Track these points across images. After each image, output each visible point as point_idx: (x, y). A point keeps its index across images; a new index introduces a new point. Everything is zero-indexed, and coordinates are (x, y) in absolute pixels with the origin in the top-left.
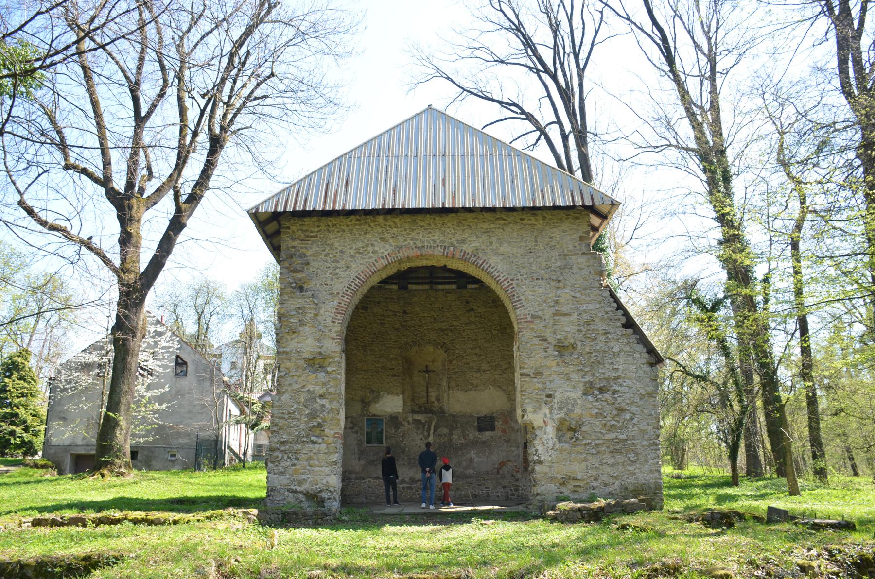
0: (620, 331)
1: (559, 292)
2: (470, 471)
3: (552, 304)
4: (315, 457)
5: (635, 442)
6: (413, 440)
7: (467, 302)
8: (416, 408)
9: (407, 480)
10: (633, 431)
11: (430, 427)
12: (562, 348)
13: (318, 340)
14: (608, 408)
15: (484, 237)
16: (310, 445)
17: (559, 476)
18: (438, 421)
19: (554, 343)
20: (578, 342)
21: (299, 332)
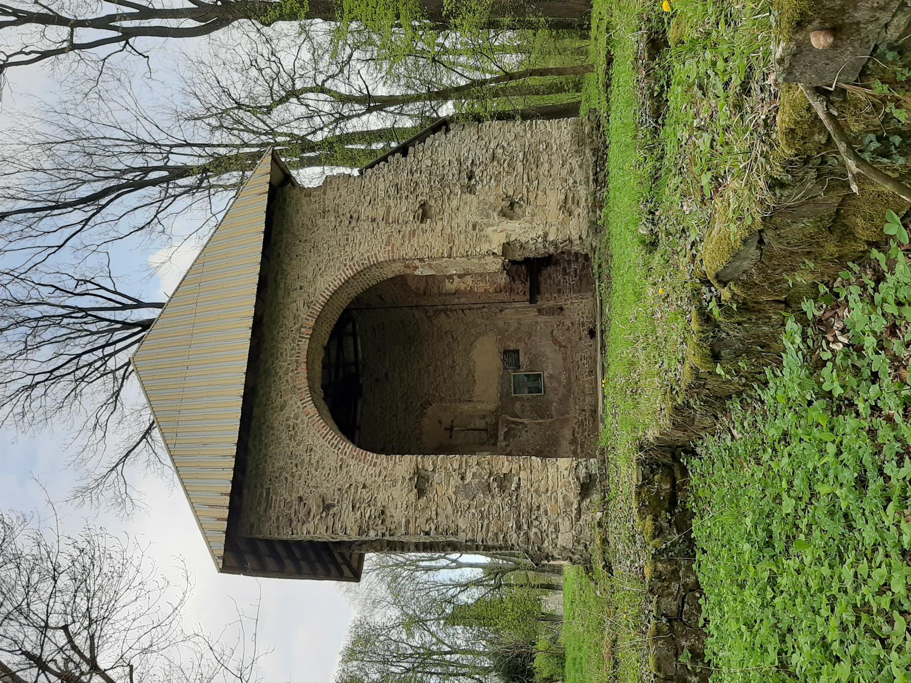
0: (410, 158)
1: (363, 217)
2: (563, 378)
3: (375, 225)
4: (536, 485)
5: (527, 144)
6: (528, 441)
7: (377, 380)
8: (492, 441)
9: (573, 448)
10: (516, 146)
11: (513, 422)
12: (424, 213)
13: (394, 483)
14: (490, 170)
15: (294, 295)
16: (521, 491)
17: (561, 217)
18: (506, 414)
19: (418, 223)
20: (419, 200)
21: (384, 507)
